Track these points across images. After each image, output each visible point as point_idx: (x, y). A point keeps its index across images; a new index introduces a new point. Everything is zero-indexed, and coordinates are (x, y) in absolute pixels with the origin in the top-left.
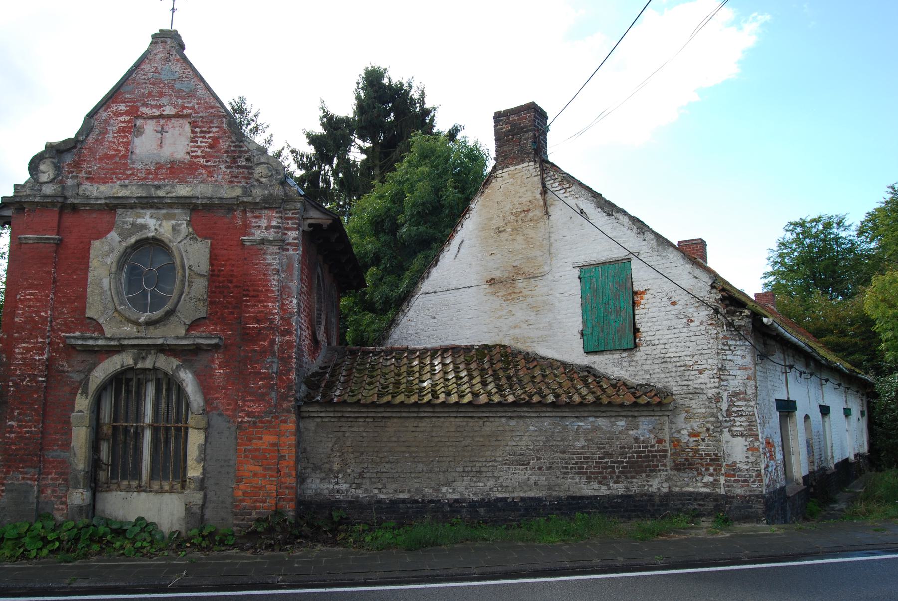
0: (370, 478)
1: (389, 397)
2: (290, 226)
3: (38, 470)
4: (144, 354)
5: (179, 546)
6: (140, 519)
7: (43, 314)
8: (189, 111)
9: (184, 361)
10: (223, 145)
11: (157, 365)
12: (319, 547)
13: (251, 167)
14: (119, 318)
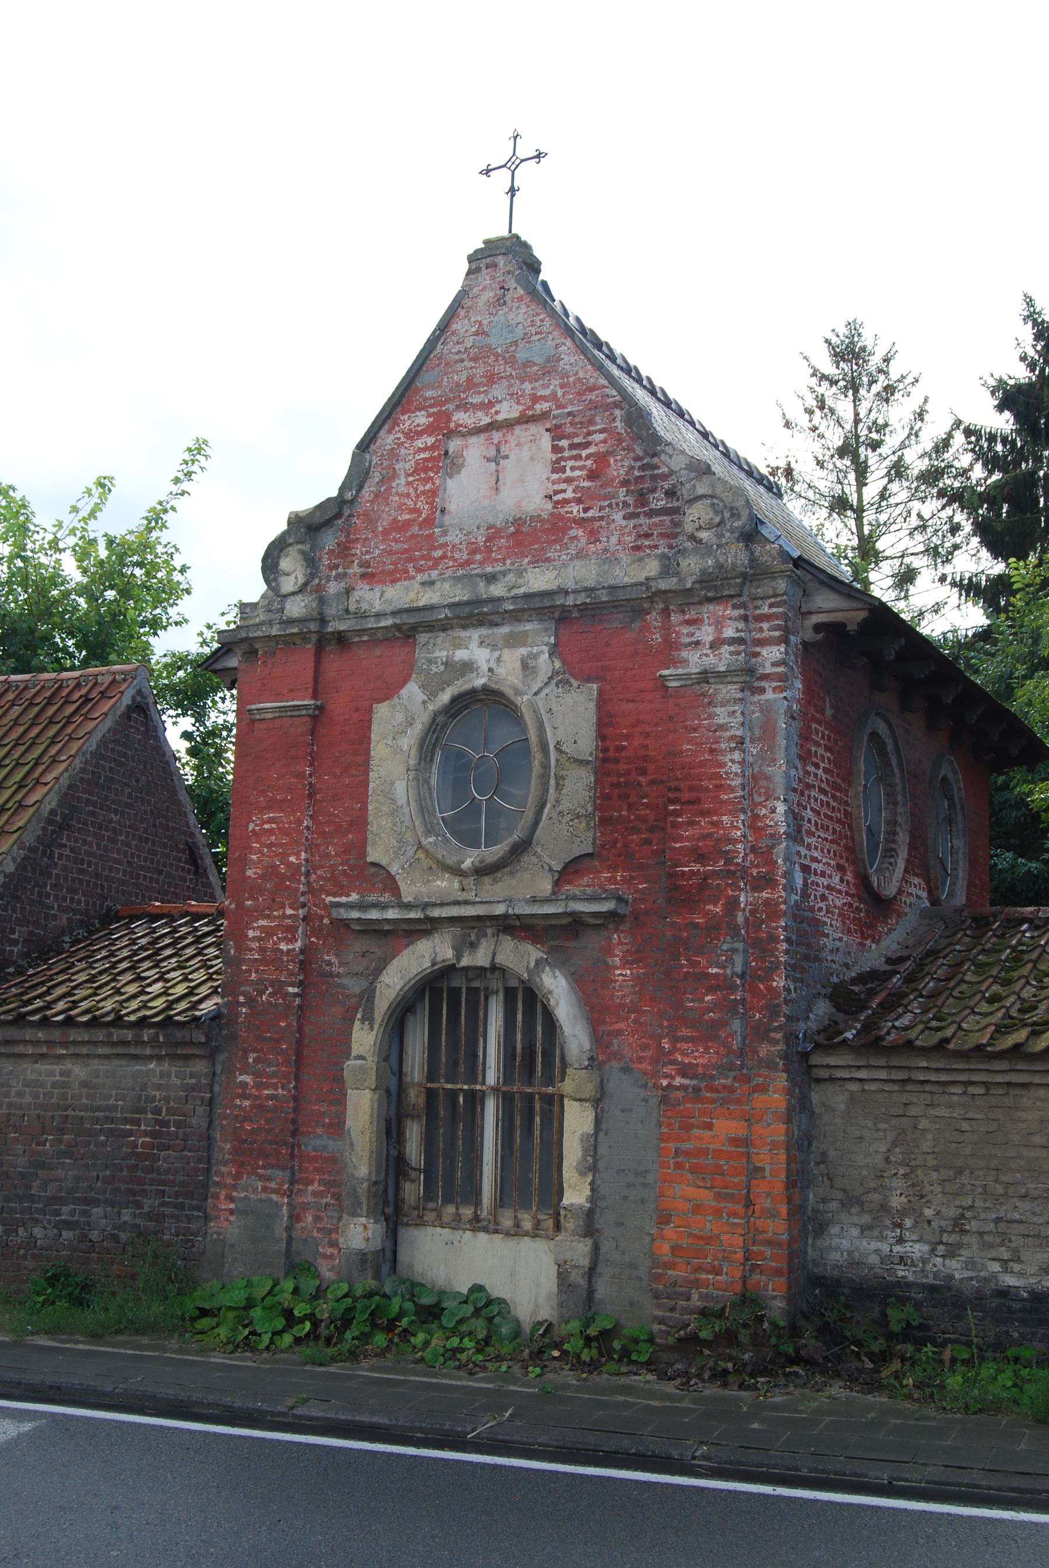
0: (981, 1234)
1: (1022, 1035)
2: (766, 634)
3: (288, 1173)
4: (473, 938)
5: (538, 1355)
6: (478, 1288)
7: (292, 859)
8: (544, 406)
9: (552, 951)
10: (618, 468)
11: (500, 959)
12: (836, 1390)
13: (676, 511)
14: (426, 863)
